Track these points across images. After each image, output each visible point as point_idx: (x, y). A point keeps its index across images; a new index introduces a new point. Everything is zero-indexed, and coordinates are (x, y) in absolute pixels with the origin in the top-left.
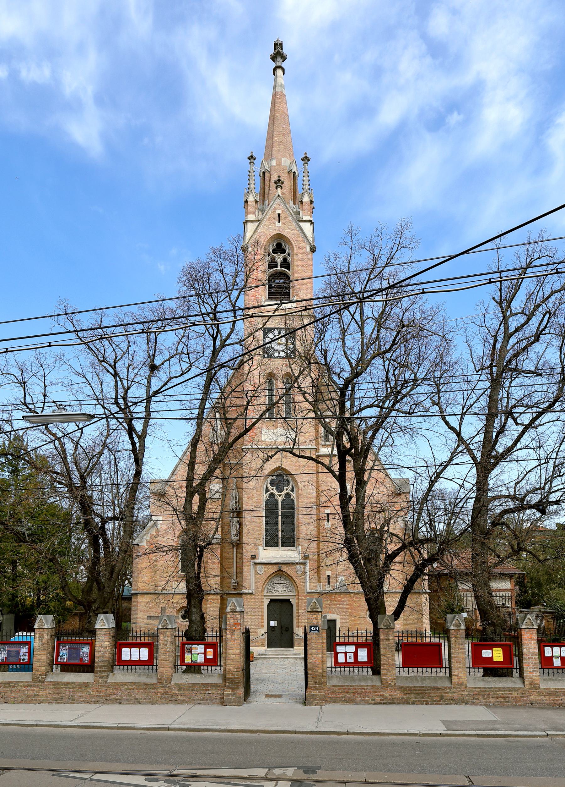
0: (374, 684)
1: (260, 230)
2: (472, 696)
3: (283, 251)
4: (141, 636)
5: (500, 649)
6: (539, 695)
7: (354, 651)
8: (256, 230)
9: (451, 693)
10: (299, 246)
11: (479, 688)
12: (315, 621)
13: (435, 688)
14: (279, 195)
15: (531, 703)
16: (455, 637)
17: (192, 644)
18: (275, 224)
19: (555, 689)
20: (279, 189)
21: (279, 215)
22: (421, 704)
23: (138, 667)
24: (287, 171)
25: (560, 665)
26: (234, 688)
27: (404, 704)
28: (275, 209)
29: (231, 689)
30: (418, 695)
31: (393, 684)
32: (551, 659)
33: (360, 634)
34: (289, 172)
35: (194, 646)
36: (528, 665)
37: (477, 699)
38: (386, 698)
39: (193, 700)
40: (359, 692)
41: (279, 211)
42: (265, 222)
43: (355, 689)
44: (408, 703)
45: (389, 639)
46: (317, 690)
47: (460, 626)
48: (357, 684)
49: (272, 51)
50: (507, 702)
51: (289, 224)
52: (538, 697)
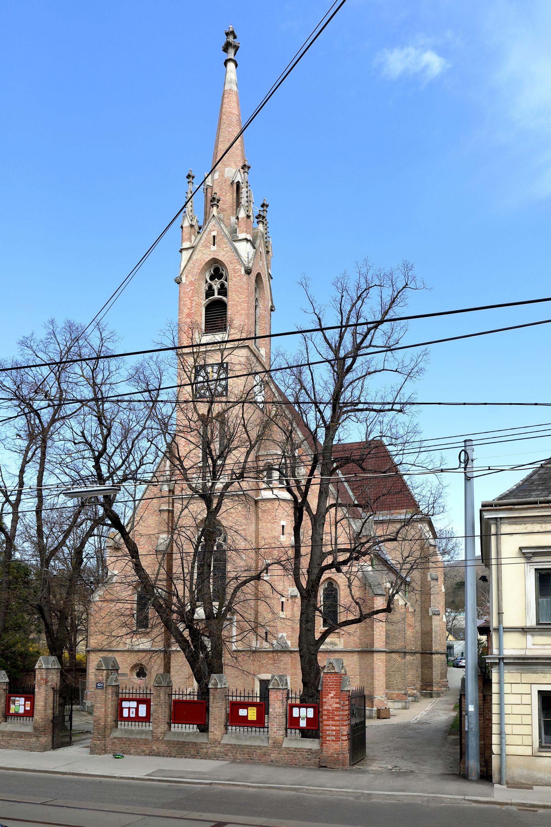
0: (147, 738)
1: (194, 257)
2: (223, 752)
3: (220, 276)
4: (296, 698)
5: (255, 708)
6: (279, 754)
7: (136, 706)
8: (190, 258)
9: (206, 748)
10: (234, 270)
11: (231, 745)
12: (101, 678)
13: (194, 743)
14: (214, 216)
15: (272, 761)
16: (213, 696)
17: (16, 697)
18: (209, 248)
19: (295, 748)
20: (215, 208)
21: (214, 237)
22: (181, 757)
23: (22, 718)
24: (229, 183)
25: (305, 726)
26: (39, 737)
27: (167, 756)
28: (211, 231)
29: (37, 737)
30: (179, 749)
31: (161, 738)
32: (298, 719)
33: (242, 695)
34: (232, 183)
35: (17, 699)
36: (273, 725)
37: (227, 755)
38: (153, 750)
39: (11, 746)
40: (133, 744)
41: (214, 233)
42: (199, 247)
43: (130, 741)
44: (171, 756)
45: (160, 696)
46: (99, 740)
47: (217, 685)
48: (133, 737)
49: (223, 40)
50: (251, 759)
51: (225, 246)
52: (278, 756)
